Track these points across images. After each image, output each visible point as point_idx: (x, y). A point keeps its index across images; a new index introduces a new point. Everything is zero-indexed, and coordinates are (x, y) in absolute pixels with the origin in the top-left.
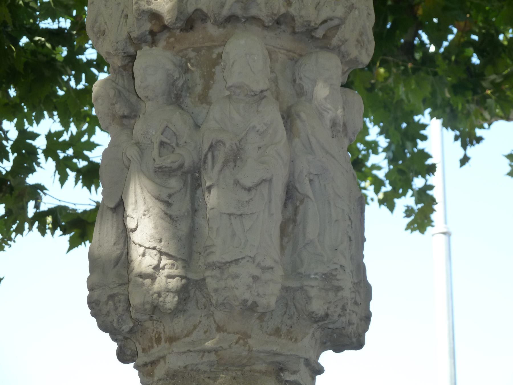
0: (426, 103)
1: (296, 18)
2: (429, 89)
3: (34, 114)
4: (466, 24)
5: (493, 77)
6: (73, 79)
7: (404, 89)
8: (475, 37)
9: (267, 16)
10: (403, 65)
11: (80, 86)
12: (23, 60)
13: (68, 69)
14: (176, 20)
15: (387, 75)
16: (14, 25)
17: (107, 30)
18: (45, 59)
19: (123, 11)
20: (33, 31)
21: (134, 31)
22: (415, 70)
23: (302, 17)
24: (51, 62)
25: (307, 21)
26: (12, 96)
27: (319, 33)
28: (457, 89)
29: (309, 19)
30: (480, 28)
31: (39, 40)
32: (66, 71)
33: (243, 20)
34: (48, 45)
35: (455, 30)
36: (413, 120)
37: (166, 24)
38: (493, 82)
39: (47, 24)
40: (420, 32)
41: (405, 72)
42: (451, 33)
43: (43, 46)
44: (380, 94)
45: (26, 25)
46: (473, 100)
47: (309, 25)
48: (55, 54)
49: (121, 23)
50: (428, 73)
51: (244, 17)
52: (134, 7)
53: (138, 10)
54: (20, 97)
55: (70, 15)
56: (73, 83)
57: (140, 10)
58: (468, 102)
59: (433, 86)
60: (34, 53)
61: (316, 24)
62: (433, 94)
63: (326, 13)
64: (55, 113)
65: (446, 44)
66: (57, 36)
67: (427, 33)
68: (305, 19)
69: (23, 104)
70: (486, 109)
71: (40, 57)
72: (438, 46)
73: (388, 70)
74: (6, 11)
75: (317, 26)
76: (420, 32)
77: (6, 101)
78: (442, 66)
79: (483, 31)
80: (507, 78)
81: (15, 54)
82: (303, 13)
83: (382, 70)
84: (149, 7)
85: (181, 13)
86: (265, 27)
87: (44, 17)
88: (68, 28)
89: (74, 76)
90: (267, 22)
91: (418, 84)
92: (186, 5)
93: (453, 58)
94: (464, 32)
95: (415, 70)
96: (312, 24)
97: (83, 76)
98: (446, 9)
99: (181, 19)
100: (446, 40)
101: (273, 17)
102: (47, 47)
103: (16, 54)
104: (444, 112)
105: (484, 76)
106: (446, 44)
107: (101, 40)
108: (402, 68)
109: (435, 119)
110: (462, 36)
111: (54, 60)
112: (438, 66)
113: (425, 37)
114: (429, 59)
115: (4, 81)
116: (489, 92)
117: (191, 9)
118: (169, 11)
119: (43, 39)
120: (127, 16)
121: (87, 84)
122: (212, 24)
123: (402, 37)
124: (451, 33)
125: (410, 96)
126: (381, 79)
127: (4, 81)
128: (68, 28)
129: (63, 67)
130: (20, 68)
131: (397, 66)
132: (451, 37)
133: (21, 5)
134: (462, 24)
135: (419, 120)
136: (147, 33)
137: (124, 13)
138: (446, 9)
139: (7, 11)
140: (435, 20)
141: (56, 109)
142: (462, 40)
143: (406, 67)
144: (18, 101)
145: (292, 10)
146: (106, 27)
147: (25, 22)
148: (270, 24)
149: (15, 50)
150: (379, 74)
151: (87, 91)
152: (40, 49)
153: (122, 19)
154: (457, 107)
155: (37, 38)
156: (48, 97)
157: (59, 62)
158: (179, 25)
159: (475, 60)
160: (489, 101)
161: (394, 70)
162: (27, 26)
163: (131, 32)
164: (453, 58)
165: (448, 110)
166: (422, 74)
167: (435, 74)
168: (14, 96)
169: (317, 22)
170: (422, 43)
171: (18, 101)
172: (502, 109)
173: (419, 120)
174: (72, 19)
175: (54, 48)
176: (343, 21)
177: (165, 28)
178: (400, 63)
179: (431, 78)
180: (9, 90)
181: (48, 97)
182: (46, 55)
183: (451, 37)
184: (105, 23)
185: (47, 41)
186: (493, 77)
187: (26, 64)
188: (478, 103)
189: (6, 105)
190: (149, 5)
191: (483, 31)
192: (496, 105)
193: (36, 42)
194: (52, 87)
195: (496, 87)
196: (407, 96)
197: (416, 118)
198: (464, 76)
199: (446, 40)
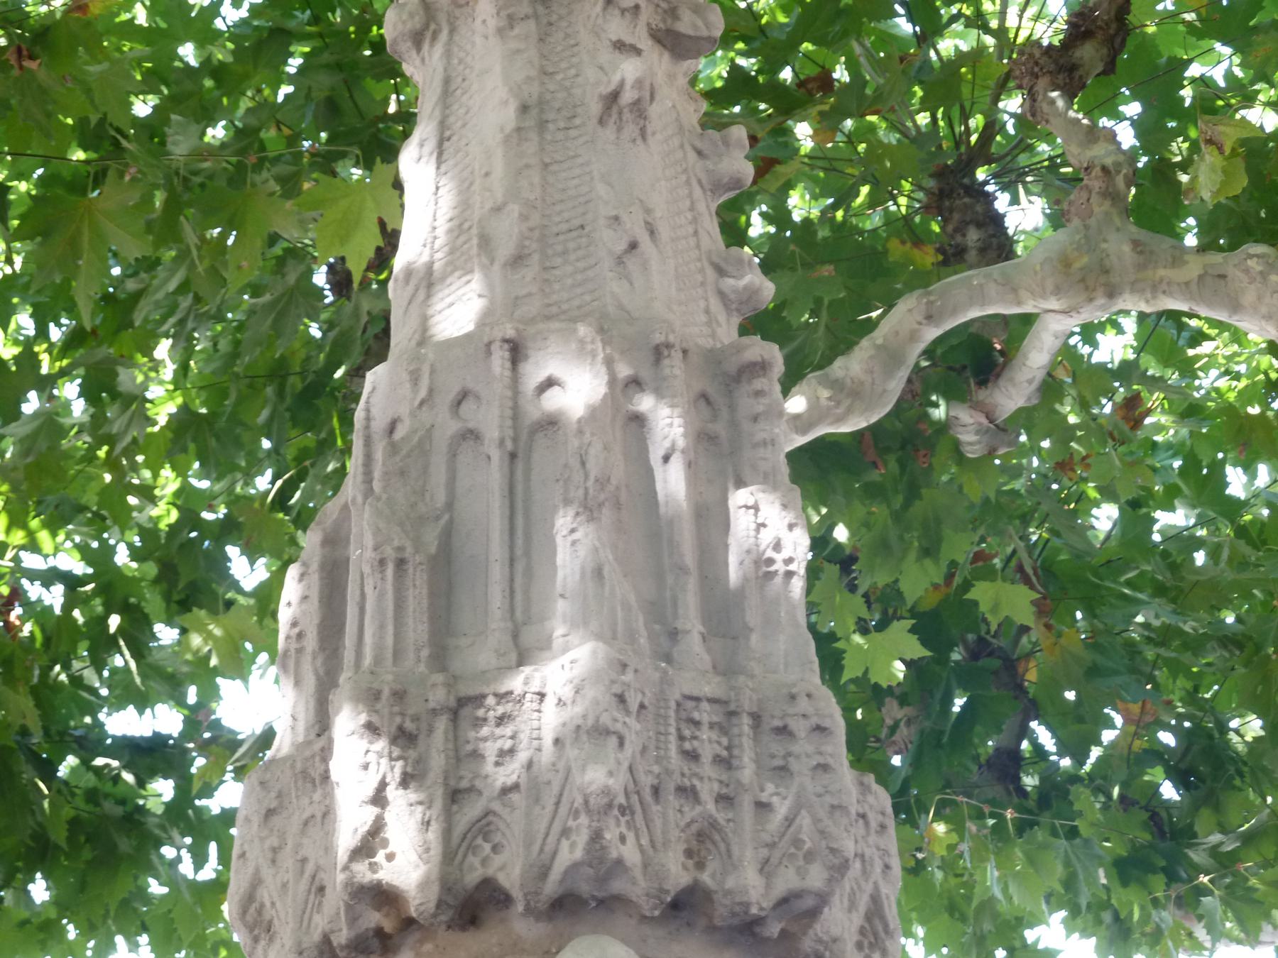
0: (1054, 902)
1: (715, 897)
2: (1059, 870)
3: (91, 944)
4: (1143, 707)
5: (1216, 838)
6: (186, 856)
7: (996, 874)
8: (1167, 738)
9: (647, 895)
10: (992, 816)
11: (208, 873)
12: (68, 812)
13: (175, 834)
14: (438, 906)
15: (954, 838)
16: (46, 732)
17: (276, 922)
18: (119, 811)
19: (314, 877)
20: (90, 743)
21: (340, 930)
22: (1023, 827)
23: (728, 893)
24: (134, 818)
25: (741, 904)
26: (38, 901)
27: (773, 929)
28: (1129, 869)
29: (745, 899)
30: (1180, 718)
31: (107, 765)
32: (170, 838)
33: (594, 904)
34: (128, 777)
35: (1118, 720)
36: (1024, 939)
37: (414, 915)
38: (1214, 851)
39: (124, 723)
40: (1034, 724)
41: (999, 830)
42: (1110, 724)
43: (117, 779)
44: (939, 875)
45: (75, 728)
46: (1168, 898)
47: (746, 913)
48: (144, 797)
49: (310, 906)
50: (1054, 833)
51: (594, 897)
52: (341, 877)
53: (348, 884)
54: (62, 904)
55: (180, 702)
56: (186, 867)
57: (353, 884)
58: (1155, 902)
59: (1067, 864)
60: (92, 796)
61: (761, 909)
62: (1070, 883)
63: (787, 881)
64: (144, 939)
65: (1096, 752)
66: (150, 755)
67: (1050, 728)
68: (737, 900)
69: (65, 921)
70: (1200, 918)
71: (109, 807)
72: (1080, 759)
73: (957, 826)
74: (28, 703)
75: (763, 914)
76: (1034, 724)
77: (25, 914)
78: (1088, 805)
79: (1187, 724)
80: (1249, 839)
81: (46, 804)
82: (730, 883)
83: (940, 828)
84: (376, 876)
85: (449, 889)
86: (644, 919)
87: (117, 704)
88: (176, 735)
89: (191, 849)
90: (647, 907)
91: (1031, 860)
92: (461, 870)
93: (1116, 791)
94: (1142, 724)
95: (1023, 827)
96: (754, 910)
97: (213, 847)
98: (1094, 672)
99: (447, 904)
100: (1098, 743)
101: (663, 896)
102: (126, 783)
103: (50, 803)
104: (1099, 922)
105: (1195, 836)
106: (1096, 752)
107: (263, 943)
108: (991, 822)
109: (1077, 935)
110: (1136, 735)
111: (142, 810)
112: (1080, 814)
113: (1045, 738)
114: (1056, 791)
115: (20, 864)
116: (1204, 879)
117: (472, 878)
118: (424, 885)
119: (115, 763)
120: (321, 889)
121: (220, 868)
122: (523, 915)
123: (989, 737)
124: (1110, 724)
125: (1012, 889)
126: (940, 851)
127: (20, 864)
128: (176, 735)
129: (163, 828)
130: (59, 835)
131: (980, 816)
132: (1108, 736)
133: (62, 682)
134: (1135, 708)
135: (1038, 941)
136: (371, 933)
137: (317, 883)
138: (1094, 672)
139: (31, 703)
140: (1070, 695)
141: (144, 928)
142: (1138, 745)
143: (1001, 818)
144: (53, 914)
145: (706, 878)
146: (273, 912)
147: (72, 723)
148: (657, 913)
149: (46, 792)
150: (934, 837)
151: (218, 887)
152: (108, 787)
153: (312, 897)
154: (1131, 913)
155: (99, 761)
156: (125, 904)
157: (155, 815)
158: (444, 918)
159: (1169, 791)
160: (1206, 900)
161: (972, 827)
162: (77, 733)
163: (333, 932)
164: (1116, 791)
165: (1107, 917)
166: (1040, 835)
167: (1073, 833)
168: (43, 903)
169: (764, 905)
170: (1039, 750)
171: (53, 914)
172: (1240, 921)
173: (1038, 941)
174: (186, 712)
175: (141, 783)
176: (823, 899)
177: (409, 923)
178: (987, 810)
179: (1063, 843)
180: (31, 887)
181: (125, 904)
182: (122, 802)
183: (1108, 736)
184: (273, 904)
185: (126, 767)
186: (1216, 838)
187: (74, 824)
188: (1180, 902)
189: (24, 923)
190: (375, 872)
191: (1187, 724)
192: (1225, 912)
193: (98, 771)
194: (136, 878)
195: (1224, 862)
196: (1005, 890)
197: (1030, 935)
198: (1144, 837)
199: (1098, 743)
